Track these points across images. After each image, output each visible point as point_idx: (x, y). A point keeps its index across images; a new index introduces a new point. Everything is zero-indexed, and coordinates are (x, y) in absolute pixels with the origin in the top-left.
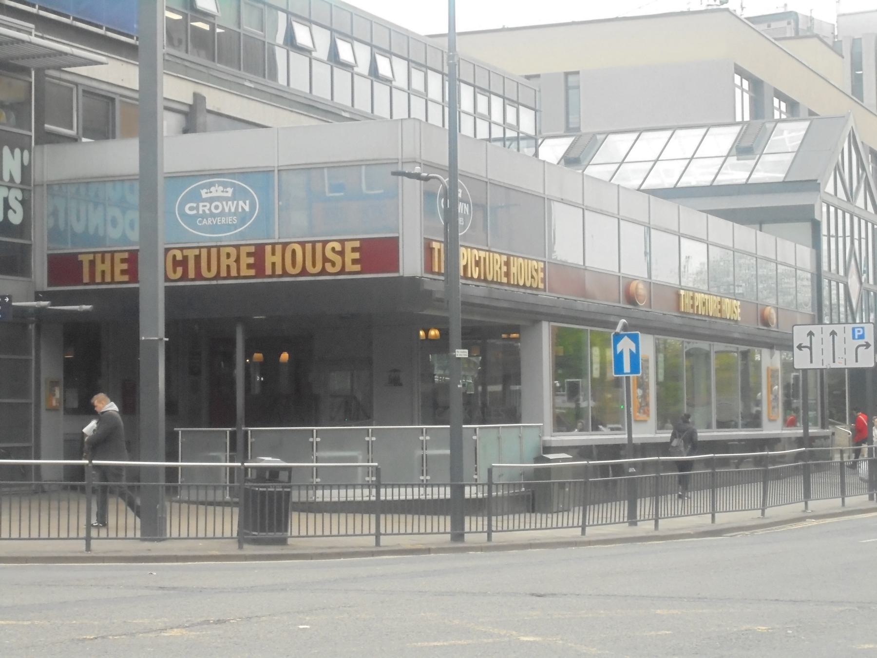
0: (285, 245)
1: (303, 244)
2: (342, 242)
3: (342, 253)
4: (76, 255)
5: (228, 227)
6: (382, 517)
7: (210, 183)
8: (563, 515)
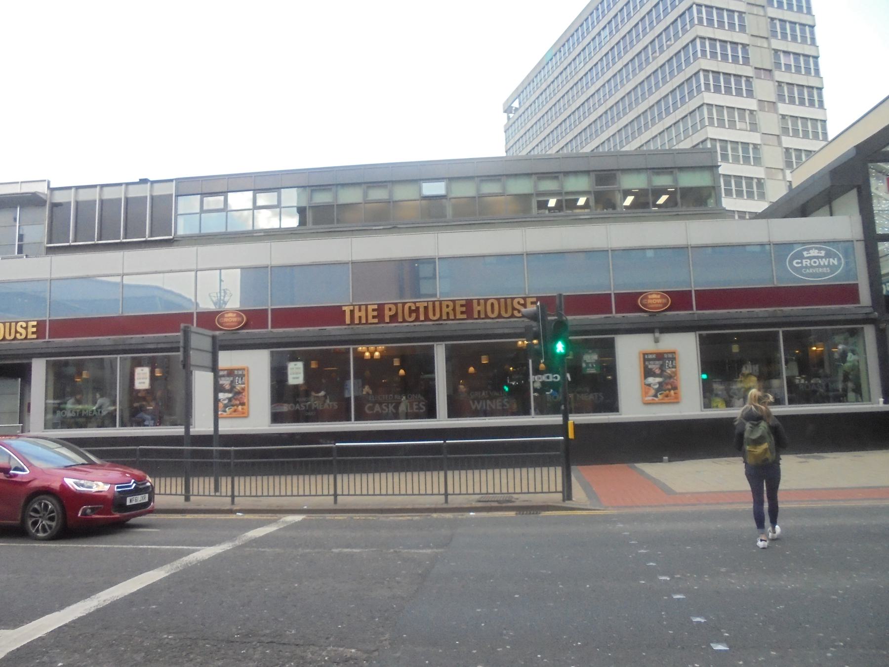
0: (486, 300)
1: (498, 300)
2: (524, 299)
3: (26, 328)
4: (340, 307)
5: (825, 274)
6: (236, 479)
7: (810, 247)
8: (210, 481)
